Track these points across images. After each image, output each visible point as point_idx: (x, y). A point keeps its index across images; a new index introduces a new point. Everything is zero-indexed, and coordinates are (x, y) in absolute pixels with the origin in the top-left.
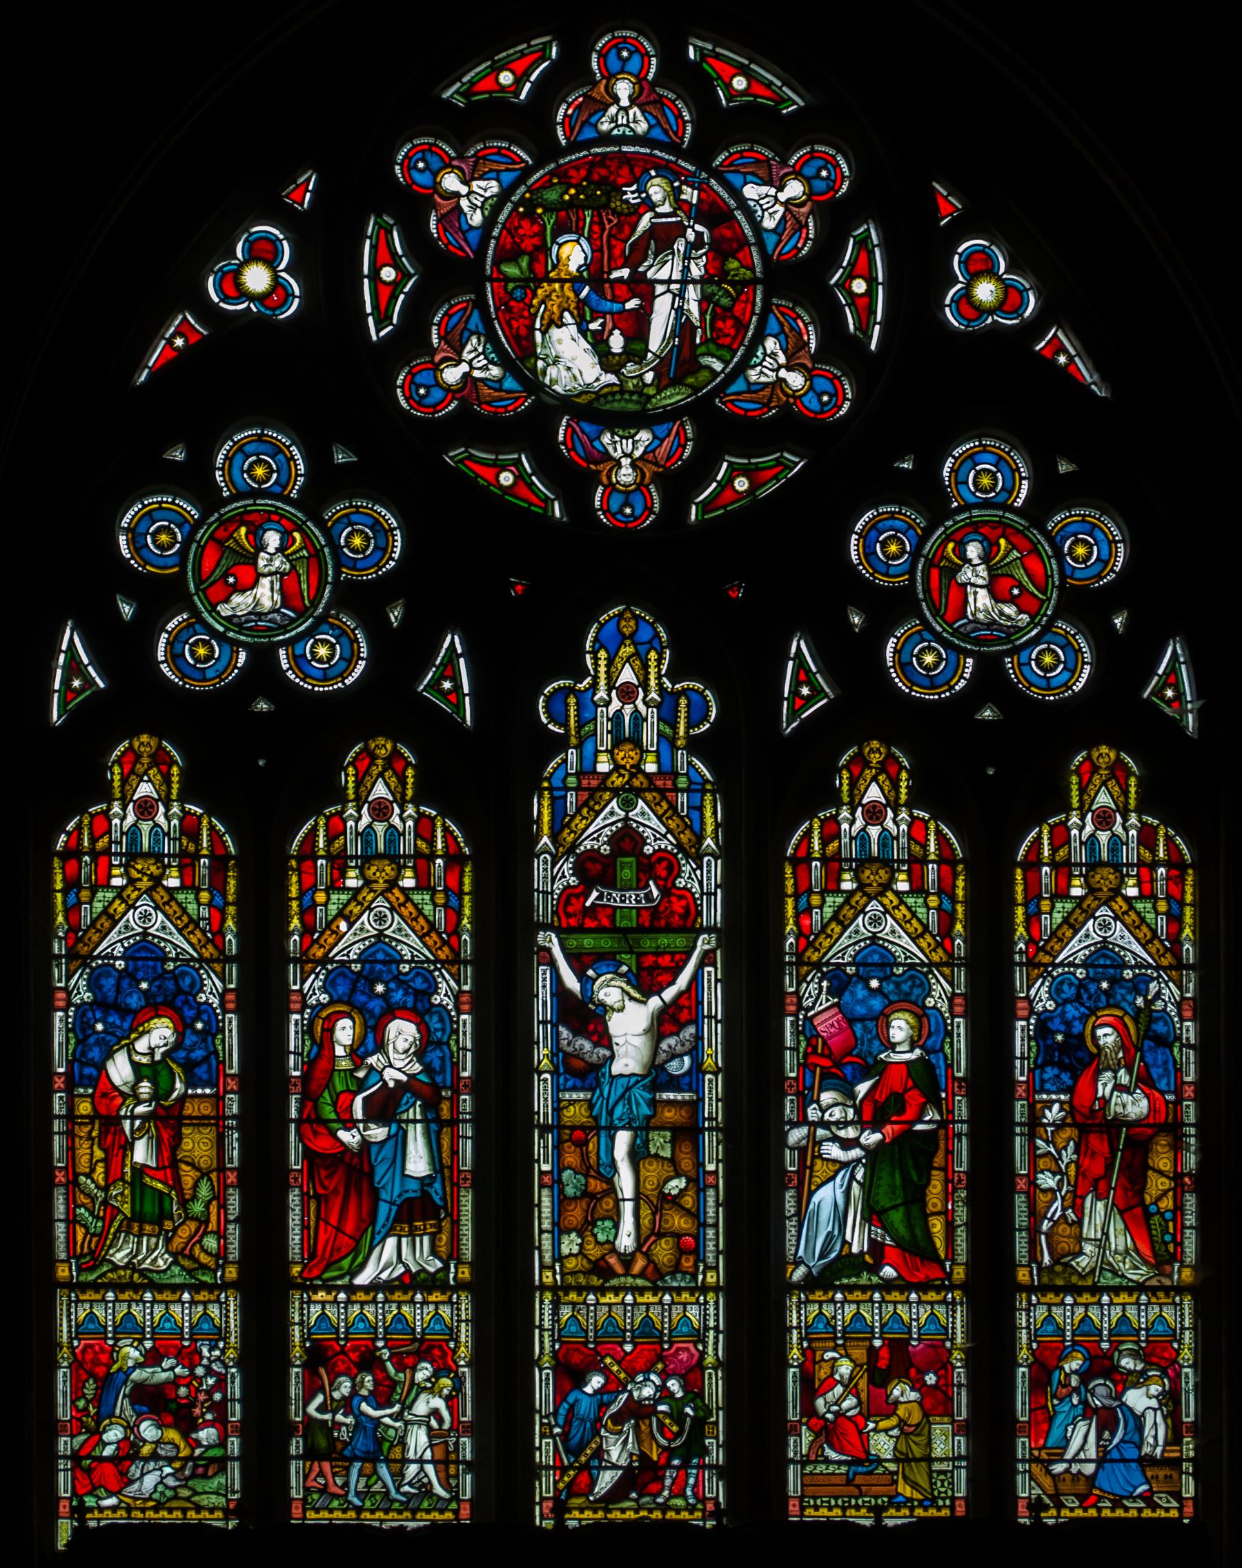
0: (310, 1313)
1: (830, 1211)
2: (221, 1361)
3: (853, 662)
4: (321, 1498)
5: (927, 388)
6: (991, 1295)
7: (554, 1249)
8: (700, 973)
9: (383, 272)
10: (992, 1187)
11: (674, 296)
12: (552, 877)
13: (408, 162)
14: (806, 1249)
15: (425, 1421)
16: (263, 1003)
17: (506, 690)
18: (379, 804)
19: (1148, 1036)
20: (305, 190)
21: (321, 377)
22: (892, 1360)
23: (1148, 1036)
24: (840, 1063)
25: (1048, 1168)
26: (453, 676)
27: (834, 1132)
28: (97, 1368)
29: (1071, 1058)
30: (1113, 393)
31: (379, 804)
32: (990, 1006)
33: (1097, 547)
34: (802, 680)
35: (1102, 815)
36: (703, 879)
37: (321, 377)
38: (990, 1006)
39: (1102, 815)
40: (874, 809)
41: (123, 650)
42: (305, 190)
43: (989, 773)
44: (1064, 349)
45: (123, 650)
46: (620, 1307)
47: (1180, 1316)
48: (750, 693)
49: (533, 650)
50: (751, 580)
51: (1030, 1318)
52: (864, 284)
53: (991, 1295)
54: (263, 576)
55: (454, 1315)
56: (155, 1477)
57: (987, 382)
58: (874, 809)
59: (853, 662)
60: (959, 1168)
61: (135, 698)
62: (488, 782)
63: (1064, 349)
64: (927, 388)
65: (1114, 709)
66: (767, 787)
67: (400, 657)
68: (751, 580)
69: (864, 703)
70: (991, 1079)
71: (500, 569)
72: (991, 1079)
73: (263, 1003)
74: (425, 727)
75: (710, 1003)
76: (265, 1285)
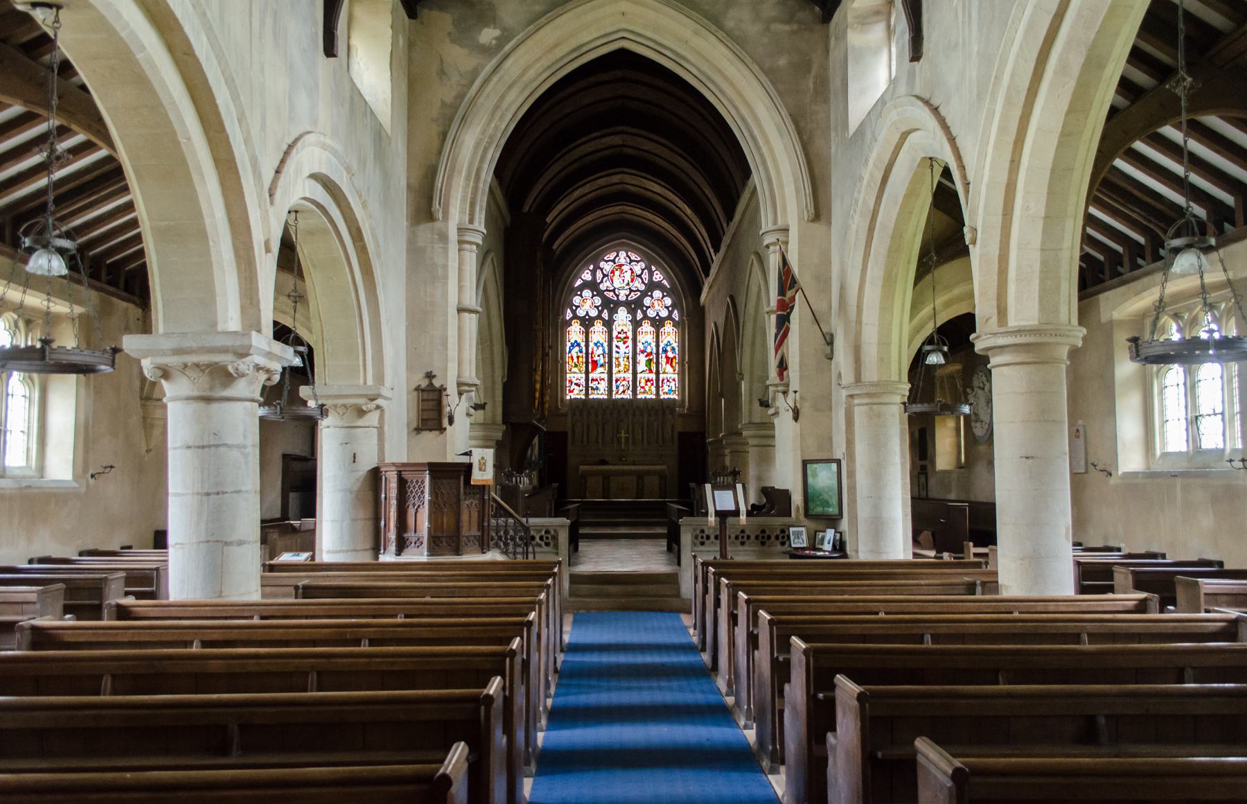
0: (591, 376)
1: (641, 366)
2: (583, 381)
3: (644, 313)
4: (593, 396)
5: (652, 286)
6: (658, 373)
7: (615, 370)
8: (630, 343)
9: (599, 275)
10: (658, 363)
11: (628, 276)
12: (615, 334)
13: (602, 264)
14: (639, 370)
15: (603, 386)
16: (587, 346)
17: (610, 316)
18: (598, 327)
19: (673, 349)
20: (591, 267)
21: (593, 286)
22: (648, 380)
23: (673, 349)
24: (643, 352)
25: (663, 360)
26: (605, 315)
27: (642, 359)
28: (571, 381)
29: (665, 351)
30: (460, 740)
31: (598, 327)
32: (658, 346)
33: (668, 301)
34: (639, 315)
35: (668, 328)
36: (630, 334)
37: (593, 286)
38: (658, 346)
39: (668, 328)
40: (647, 327)
41: (574, 312)
42: (591, 267)
43: (658, 323)
44: (665, 282)
45: (574, 312)
46: (622, 375)
47: (676, 376)
48: (634, 316)
49: (613, 311)
50: (634, 306)
51: (661, 376)
52: (645, 276)
53: (658, 373)
54: (586, 304)
55: (605, 376)
56: (576, 394)
57: (659, 286)
58: (647, 327)
59: (644, 313)
60: (654, 363)
61: (575, 317)
62: (609, 324)
63: (665, 282)
64: (652, 286)
65: (669, 317)
66: (636, 324)
67: (600, 312)
68: (634, 306)
69: (645, 317)
70: (657, 354)
71: (610, 305)
72: (657, 354)
73: (587, 346)
74: (603, 319)
75: (398, 578)
76: (587, 373)
